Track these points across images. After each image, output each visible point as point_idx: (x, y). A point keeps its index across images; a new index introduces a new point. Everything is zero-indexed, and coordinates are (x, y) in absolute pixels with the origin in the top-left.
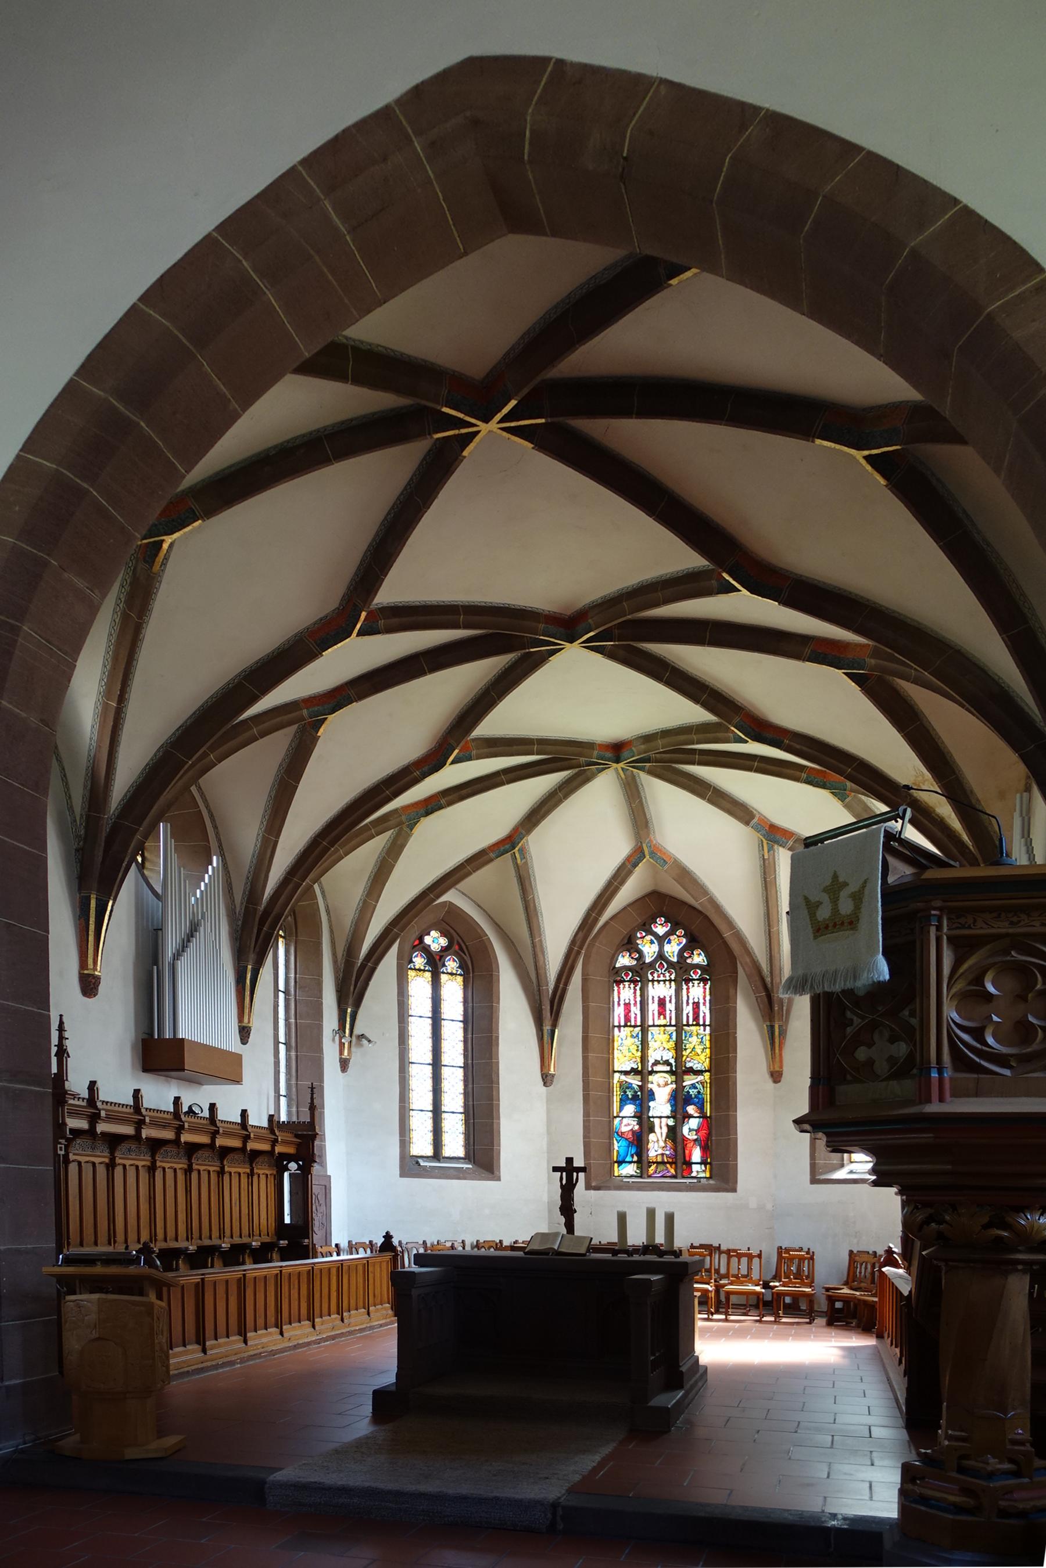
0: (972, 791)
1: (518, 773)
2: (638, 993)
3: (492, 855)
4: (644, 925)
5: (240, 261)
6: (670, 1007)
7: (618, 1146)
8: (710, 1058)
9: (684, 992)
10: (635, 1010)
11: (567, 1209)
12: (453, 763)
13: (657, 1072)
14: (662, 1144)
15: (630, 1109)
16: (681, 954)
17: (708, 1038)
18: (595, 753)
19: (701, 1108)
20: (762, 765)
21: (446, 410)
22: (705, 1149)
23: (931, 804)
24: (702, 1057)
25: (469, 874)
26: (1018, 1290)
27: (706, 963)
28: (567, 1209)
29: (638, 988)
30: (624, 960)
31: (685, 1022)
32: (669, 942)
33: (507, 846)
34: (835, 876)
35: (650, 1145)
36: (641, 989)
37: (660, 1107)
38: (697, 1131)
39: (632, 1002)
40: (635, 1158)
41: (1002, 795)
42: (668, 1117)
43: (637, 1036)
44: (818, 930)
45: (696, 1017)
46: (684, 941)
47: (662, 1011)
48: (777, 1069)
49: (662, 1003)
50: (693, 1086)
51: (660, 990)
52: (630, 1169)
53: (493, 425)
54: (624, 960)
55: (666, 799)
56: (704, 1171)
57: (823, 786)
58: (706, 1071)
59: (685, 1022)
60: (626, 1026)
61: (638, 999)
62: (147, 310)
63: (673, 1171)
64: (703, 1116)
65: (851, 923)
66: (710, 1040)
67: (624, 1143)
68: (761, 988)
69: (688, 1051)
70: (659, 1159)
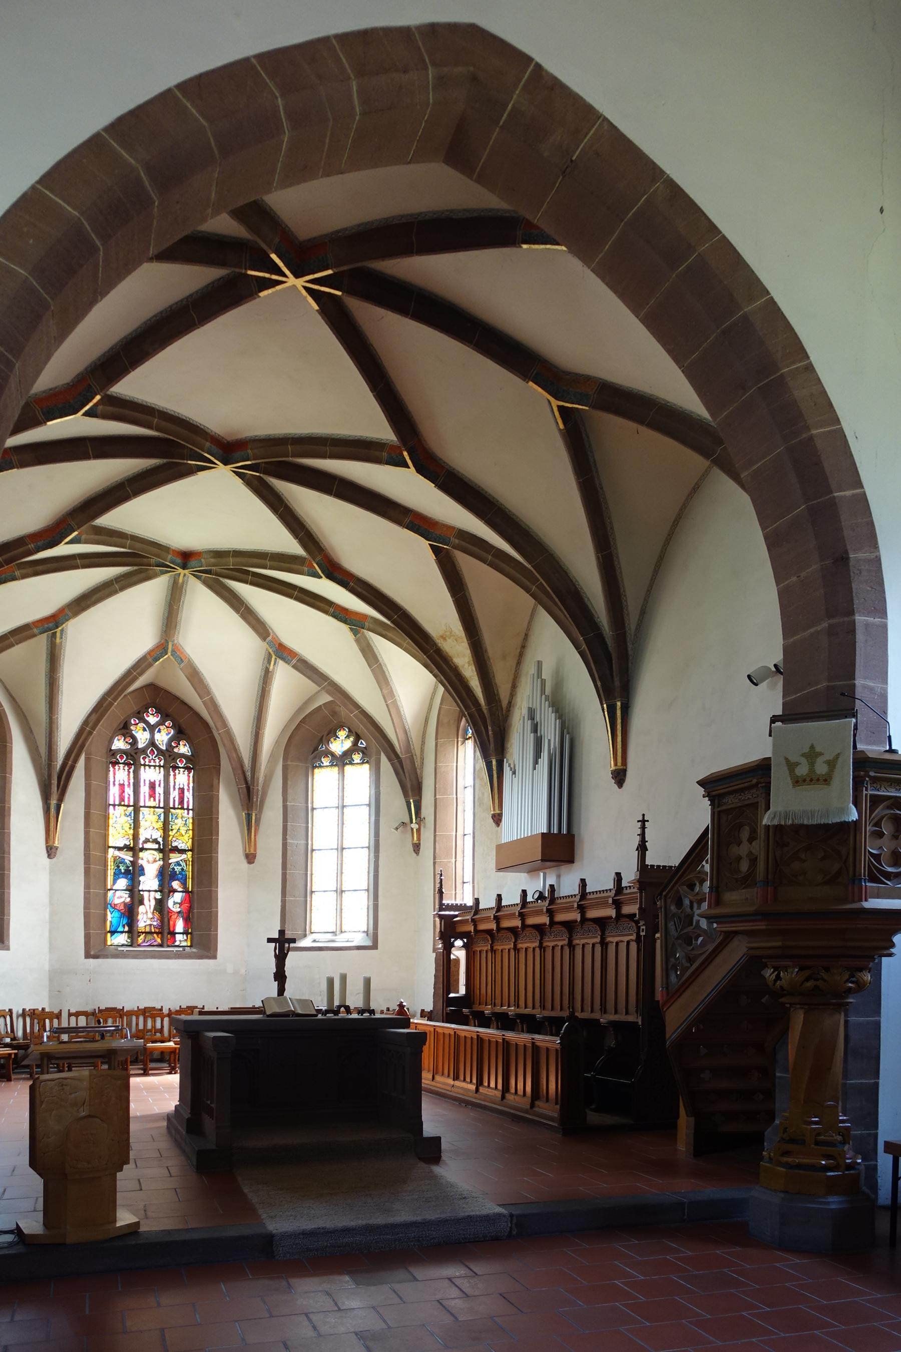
0: (486, 651)
1: (93, 560)
2: (132, 775)
3: (35, 631)
4: (139, 713)
5: (276, 98)
6: (160, 790)
7: (112, 917)
8: (193, 839)
9: (172, 778)
10: (129, 791)
11: (280, 977)
12: (67, 543)
13: (147, 849)
14: (150, 916)
15: (122, 883)
16: (169, 744)
17: (191, 821)
18: (170, 556)
19: (184, 884)
20: (300, 595)
21: (274, 256)
22: (187, 920)
23: (450, 654)
24: (186, 837)
25: (11, 646)
27: (190, 754)
28: (280, 977)
29: (131, 770)
30: (119, 744)
31: (171, 806)
32: (159, 731)
33: (51, 625)
34: (812, 747)
35: (140, 917)
36: (134, 772)
37: (149, 882)
38: (181, 904)
39: (126, 783)
40: (126, 929)
41: (504, 657)
42: (156, 891)
43: (130, 815)
44: (797, 782)
45: (181, 802)
46: (172, 732)
47: (152, 794)
48: (252, 851)
49: (152, 786)
50: (178, 864)
51: (151, 774)
52: (121, 939)
53: (300, 283)
54: (119, 744)
55: (203, 607)
56: (186, 940)
57: (345, 622)
58: (189, 850)
59: (171, 806)
60: (120, 805)
61: (132, 781)
62: (184, 101)
63: (159, 940)
64: (186, 891)
66: (193, 823)
67: (116, 914)
68: (243, 781)
69: (175, 831)
70: (148, 929)
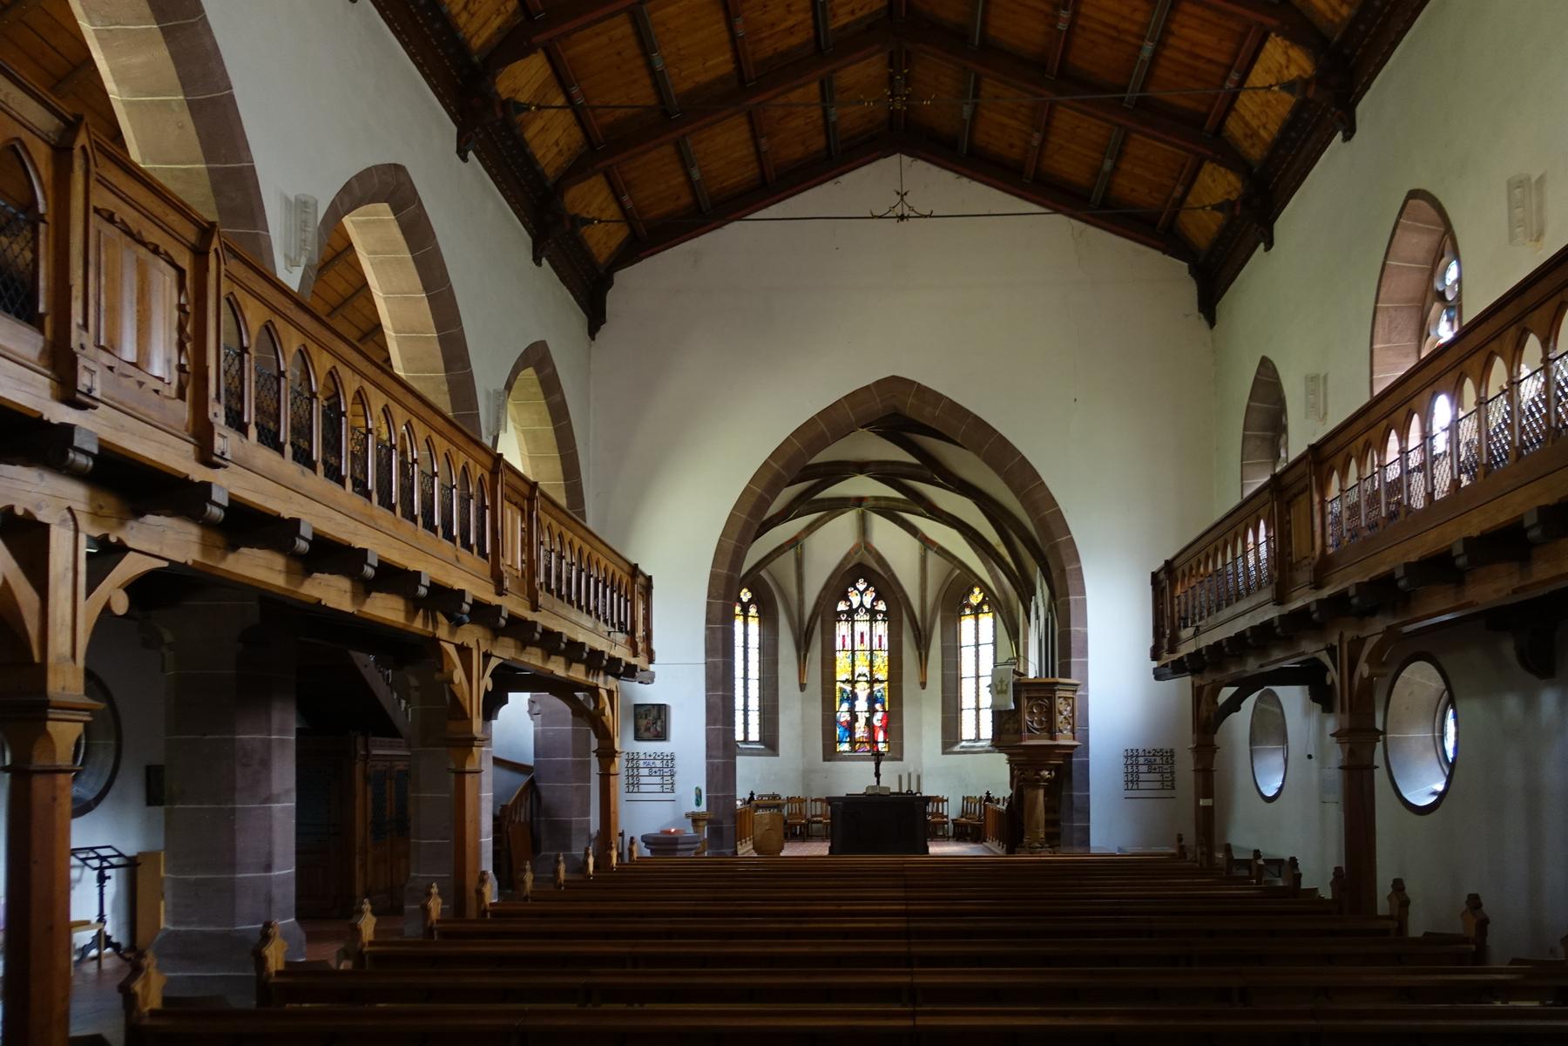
11: (877, 774)
15: (845, 706)
22: (885, 733)
26: (1041, 792)
37: (861, 705)
51: (862, 627)
52: (845, 747)
65: (1005, 692)
